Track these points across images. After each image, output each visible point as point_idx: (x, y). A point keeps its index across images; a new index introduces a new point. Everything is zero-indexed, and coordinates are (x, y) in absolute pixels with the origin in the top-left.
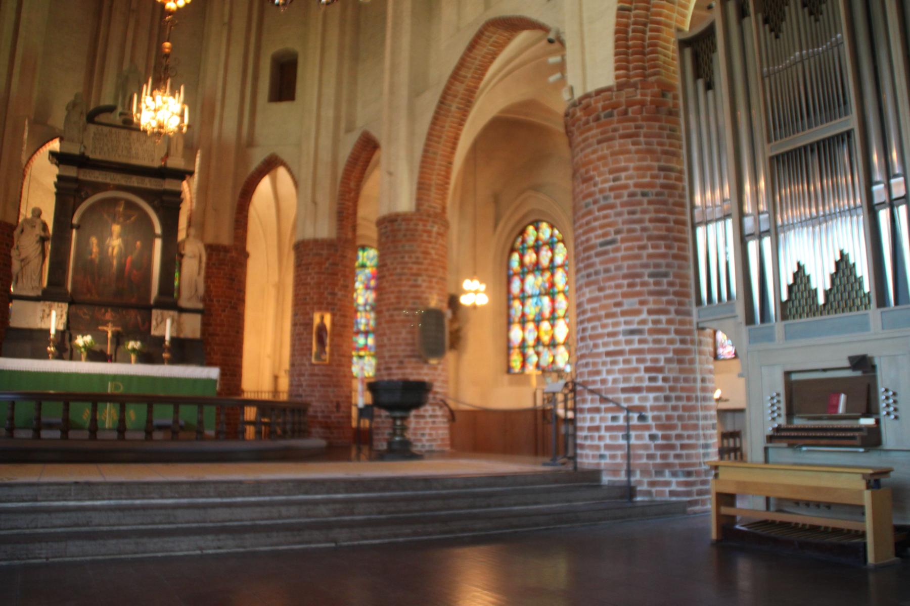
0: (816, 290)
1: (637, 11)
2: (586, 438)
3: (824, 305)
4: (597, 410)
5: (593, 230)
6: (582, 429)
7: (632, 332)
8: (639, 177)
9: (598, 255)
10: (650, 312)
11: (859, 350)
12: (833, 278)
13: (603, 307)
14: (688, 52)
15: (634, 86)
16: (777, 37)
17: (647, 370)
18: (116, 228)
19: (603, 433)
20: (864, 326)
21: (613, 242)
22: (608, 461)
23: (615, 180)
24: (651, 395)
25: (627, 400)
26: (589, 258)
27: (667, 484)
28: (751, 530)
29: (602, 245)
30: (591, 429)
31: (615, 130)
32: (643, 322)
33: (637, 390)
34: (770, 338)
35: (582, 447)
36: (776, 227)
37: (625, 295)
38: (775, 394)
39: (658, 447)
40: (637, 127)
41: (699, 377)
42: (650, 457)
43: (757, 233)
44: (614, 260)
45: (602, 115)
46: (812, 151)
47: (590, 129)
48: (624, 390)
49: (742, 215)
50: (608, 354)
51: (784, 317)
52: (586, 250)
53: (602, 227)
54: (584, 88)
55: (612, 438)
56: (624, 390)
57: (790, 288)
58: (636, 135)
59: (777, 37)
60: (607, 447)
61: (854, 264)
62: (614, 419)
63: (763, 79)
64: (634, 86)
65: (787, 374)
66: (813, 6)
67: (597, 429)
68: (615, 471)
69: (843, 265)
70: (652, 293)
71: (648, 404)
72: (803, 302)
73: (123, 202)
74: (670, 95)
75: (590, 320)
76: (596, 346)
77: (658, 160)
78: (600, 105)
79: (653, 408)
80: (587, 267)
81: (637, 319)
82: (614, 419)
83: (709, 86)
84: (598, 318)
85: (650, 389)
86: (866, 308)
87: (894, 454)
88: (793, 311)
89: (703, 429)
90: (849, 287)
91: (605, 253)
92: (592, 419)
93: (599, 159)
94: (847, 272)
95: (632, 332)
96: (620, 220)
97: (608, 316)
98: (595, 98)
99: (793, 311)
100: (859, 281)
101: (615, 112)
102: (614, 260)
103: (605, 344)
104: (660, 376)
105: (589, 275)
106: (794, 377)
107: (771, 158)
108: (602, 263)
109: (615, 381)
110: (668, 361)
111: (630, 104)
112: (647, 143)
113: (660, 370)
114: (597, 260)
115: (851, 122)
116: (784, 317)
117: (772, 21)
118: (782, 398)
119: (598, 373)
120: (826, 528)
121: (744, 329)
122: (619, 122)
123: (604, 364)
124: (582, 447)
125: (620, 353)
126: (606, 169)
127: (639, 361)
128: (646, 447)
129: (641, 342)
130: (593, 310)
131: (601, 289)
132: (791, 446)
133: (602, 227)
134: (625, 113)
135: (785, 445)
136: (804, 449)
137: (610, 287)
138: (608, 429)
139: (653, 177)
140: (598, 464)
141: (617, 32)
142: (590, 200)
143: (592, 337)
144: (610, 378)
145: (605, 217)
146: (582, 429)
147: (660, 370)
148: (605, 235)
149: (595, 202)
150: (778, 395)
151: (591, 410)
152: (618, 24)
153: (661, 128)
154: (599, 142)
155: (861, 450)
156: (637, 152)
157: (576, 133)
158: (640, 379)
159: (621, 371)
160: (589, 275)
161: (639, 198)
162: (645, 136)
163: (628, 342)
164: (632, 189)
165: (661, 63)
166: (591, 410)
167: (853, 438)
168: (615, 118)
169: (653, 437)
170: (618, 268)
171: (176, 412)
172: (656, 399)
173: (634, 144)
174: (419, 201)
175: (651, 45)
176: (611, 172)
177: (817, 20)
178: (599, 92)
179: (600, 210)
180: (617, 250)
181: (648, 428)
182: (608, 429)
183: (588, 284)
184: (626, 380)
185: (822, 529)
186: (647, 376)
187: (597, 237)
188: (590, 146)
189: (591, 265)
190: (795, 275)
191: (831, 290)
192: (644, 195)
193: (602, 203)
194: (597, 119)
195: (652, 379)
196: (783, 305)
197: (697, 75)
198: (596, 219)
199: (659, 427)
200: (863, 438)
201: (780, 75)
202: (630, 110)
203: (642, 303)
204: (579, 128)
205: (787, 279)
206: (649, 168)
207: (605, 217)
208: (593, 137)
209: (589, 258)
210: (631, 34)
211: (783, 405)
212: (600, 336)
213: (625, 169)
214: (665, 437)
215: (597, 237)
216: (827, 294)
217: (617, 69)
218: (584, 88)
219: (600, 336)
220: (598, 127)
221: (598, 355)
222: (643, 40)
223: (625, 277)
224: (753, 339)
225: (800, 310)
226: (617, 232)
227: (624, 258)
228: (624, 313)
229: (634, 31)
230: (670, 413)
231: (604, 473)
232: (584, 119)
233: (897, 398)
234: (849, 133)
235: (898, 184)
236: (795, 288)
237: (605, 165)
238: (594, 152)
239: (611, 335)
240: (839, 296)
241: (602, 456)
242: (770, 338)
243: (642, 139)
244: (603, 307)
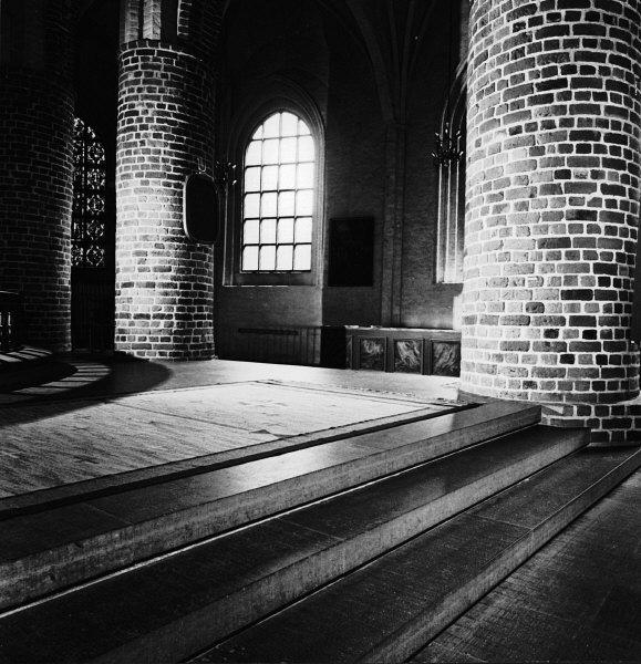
7: (581, 215)
10: (606, 189)
17: (598, 268)
24: (602, 303)
29: (541, 87)
32: (596, 202)
33: (585, 295)
37: (575, 162)
53: (544, 60)
70: (607, 163)
71: (598, 315)
73: (384, 321)
79: (604, 322)
81: (588, 197)
85: (602, 296)
95: (581, 215)
96: (572, 52)
110: (620, 257)
114: (534, 109)
127: (589, 256)
148: (547, 72)
158: (590, 281)
172: (607, 309)
181: (596, 347)
186: (136, 109)
199: (609, 347)
201: (141, 32)
226: (570, 69)
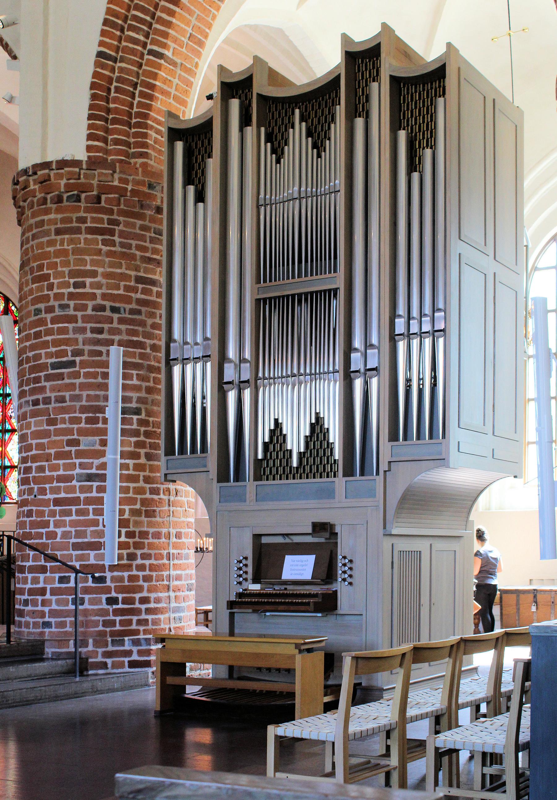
0: (291, 451)
1: (123, 65)
2: (26, 603)
3: (297, 468)
4: (43, 570)
5: (45, 345)
6: (22, 592)
8: (109, 287)
9: (48, 378)
11: (322, 517)
12: (308, 440)
13: (53, 444)
14: (179, 146)
15: (112, 166)
16: (278, 161)
19: (48, 596)
20: (330, 494)
21: (72, 364)
23: (76, 285)
25: (80, 558)
26: (37, 380)
27: (129, 653)
28: (213, 700)
29: (55, 366)
30: (31, 592)
31: (83, 220)
34: (242, 498)
35: (21, 613)
36: (257, 378)
38: (241, 558)
39: (137, 612)
40: (110, 222)
41: (173, 531)
42: (106, 624)
43: (237, 381)
44: (72, 387)
45: (65, 196)
46: (306, 300)
47: (47, 212)
48: (76, 547)
49: (223, 358)
50: (57, 502)
51: (258, 477)
52: (33, 369)
53: (56, 343)
54: (44, 149)
55: (58, 602)
56: (76, 547)
57: (266, 445)
58: (112, 233)
59: (278, 161)
60: (53, 613)
61: (328, 429)
62: (62, 580)
63: (258, 207)
64: (112, 166)
65: (257, 537)
66: (319, 138)
67: (43, 592)
68: (62, 642)
69: (318, 429)
72: (278, 462)
74: (158, 188)
75: (35, 459)
76: (43, 491)
77: (137, 269)
78: (63, 182)
80: (33, 391)
82: (62, 580)
83: (200, 197)
84: (48, 458)
86: (335, 476)
87: (347, 618)
88: (268, 471)
89: (174, 591)
90: (321, 453)
91: (61, 377)
92: (35, 580)
93: (58, 254)
94: (321, 436)
96: (80, 337)
97: (60, 455)
98: (55, 171)
99: (268, 471)
100: (330, 446)
101: (83, 196)
102: (72, 387)
103: (56, 490)
105: (36, 403)
106: (264, 540)
107: (258, 301)
108: (53, 389)
109: (66, 535)
111: (105, 189)
115: (339, 282)
116: (258, 477)
117: (276, 140)
118: (250, 562)
119: (46, 524)
120: (261, 691)
121: (215, 485)
122: (87, 210)
123: (53, 514)
124: (21, 613)
125: (75, 501)
126: (66, 270)
128: (105, 613)
130: (40, 446)
131: (52, 422)
132: (255, 611)
133: (56, 343)
134: (98, 199)
135: (250, 610)
136: (268, 614)
137: (63, 421)
138: (54, 592)
139: (128, 289)
140: (42, 633)
141: (93, 86)
142: (42, 306)
143: (36, 480)
144: (59, 531)
145: (64, 331)
146: (22, 592)
148: (58, 354)
149: (50, 310)
150: (246, 558)
151: (32, 569)
152: (96, 75)
153: (143, 228)
154: (58, 232)
155: (320, 615)
156: (110, 254)
157: (28, 213)
159: (73, 524)
160: (36, 403)
161: (108, 313)
162: (122, 234)
163: (83, 489)
164: (99, 301)
165: (151, 142)
166: (32, 569)
167: (308, 604)
168: (83, 204)
169: (112, 601)
170: (78, 398)
173: (105, 243)
175: (138, 115)
176: (72, 274)
177: (319, 156)
178: (62, 164)
179: (54, 321)
180: (76, 375)
182: (54, 592)
183: (34, 414)
184: (79, 534)
185: (278, 693)
187: (50, 355)
188: (47, 233)
189: (42, 389)
190: (272, 433)
191: (304, 453)
192: (114, 310)
193: (58, 312)
194: (59, 200)
196: (258, 463)
197: (188, 181)
198: (49, 332)
200: (315, 603)
202: (103, 197)
204: (31, 206)
205: (263, 436)
206: (124, 277)
207: (64, 331)
208: (50, 222)
209: (37, 380)
210: (113, 94)
211: (250, 569)
212: (50, 480)
213: (94, 274)
214: (131, 601)
215: (50, 355)
216: (301, 456)
217: (90, 137)
219: (50, 480)
220: (57, 211)
221: (46, 503)
222: (131, 106)
223: (83, 409)
224: (223, 498)
225: (274, 471)
227: (83, 387)
228: (80, 454)
229: (117, 90)
230: (135, 572)
231: (47, 644)
232: (39, 195)
233: (353, 566)
234: (336, 290)
235: (374, 354)
236: (271, 447)
237: (66, 264)
238: (51, 243)
239: (60, 479)
240: (311, 461)
241: (47, 625)
242: (242, 498)
243: (116, 238)
244: (53, 444)
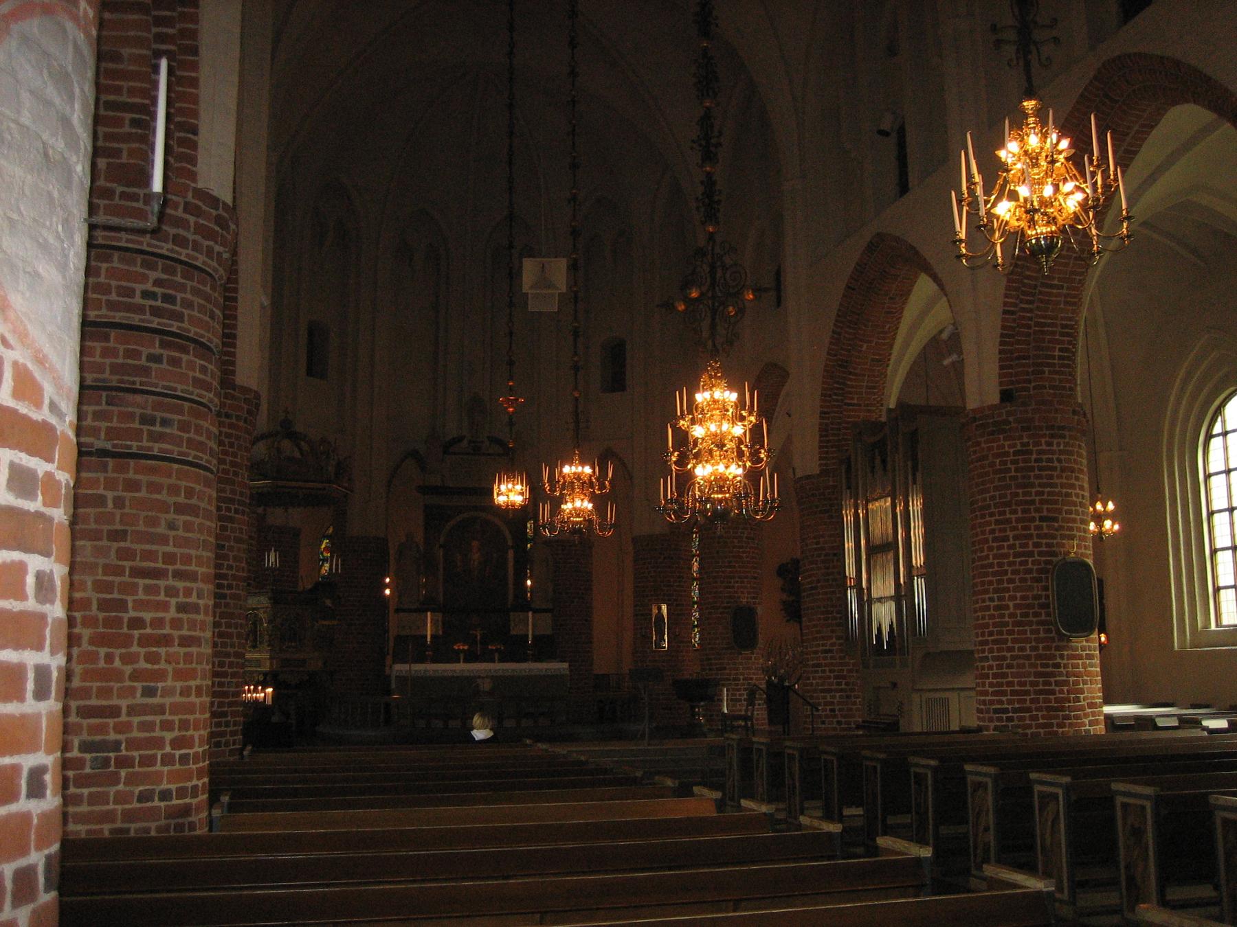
7: (826, 652)
17: (836, 677)
18: (475, 544)
22: (145, 351)
32: (833, 645)
54: (1206, 130)
95: (826, 652)
104: (844, 682)
110: (850, 671)
112: (1029, 494)
113: (844, 677)
127: (830, 671)
129: (832, 658)
147: (844, 677)
171: (880, 600)
172: (841, 697)
174: (846, 816)
181: (835, 716)
195: (839, 684)
203: (832, 631)
218: (1206, 130)
